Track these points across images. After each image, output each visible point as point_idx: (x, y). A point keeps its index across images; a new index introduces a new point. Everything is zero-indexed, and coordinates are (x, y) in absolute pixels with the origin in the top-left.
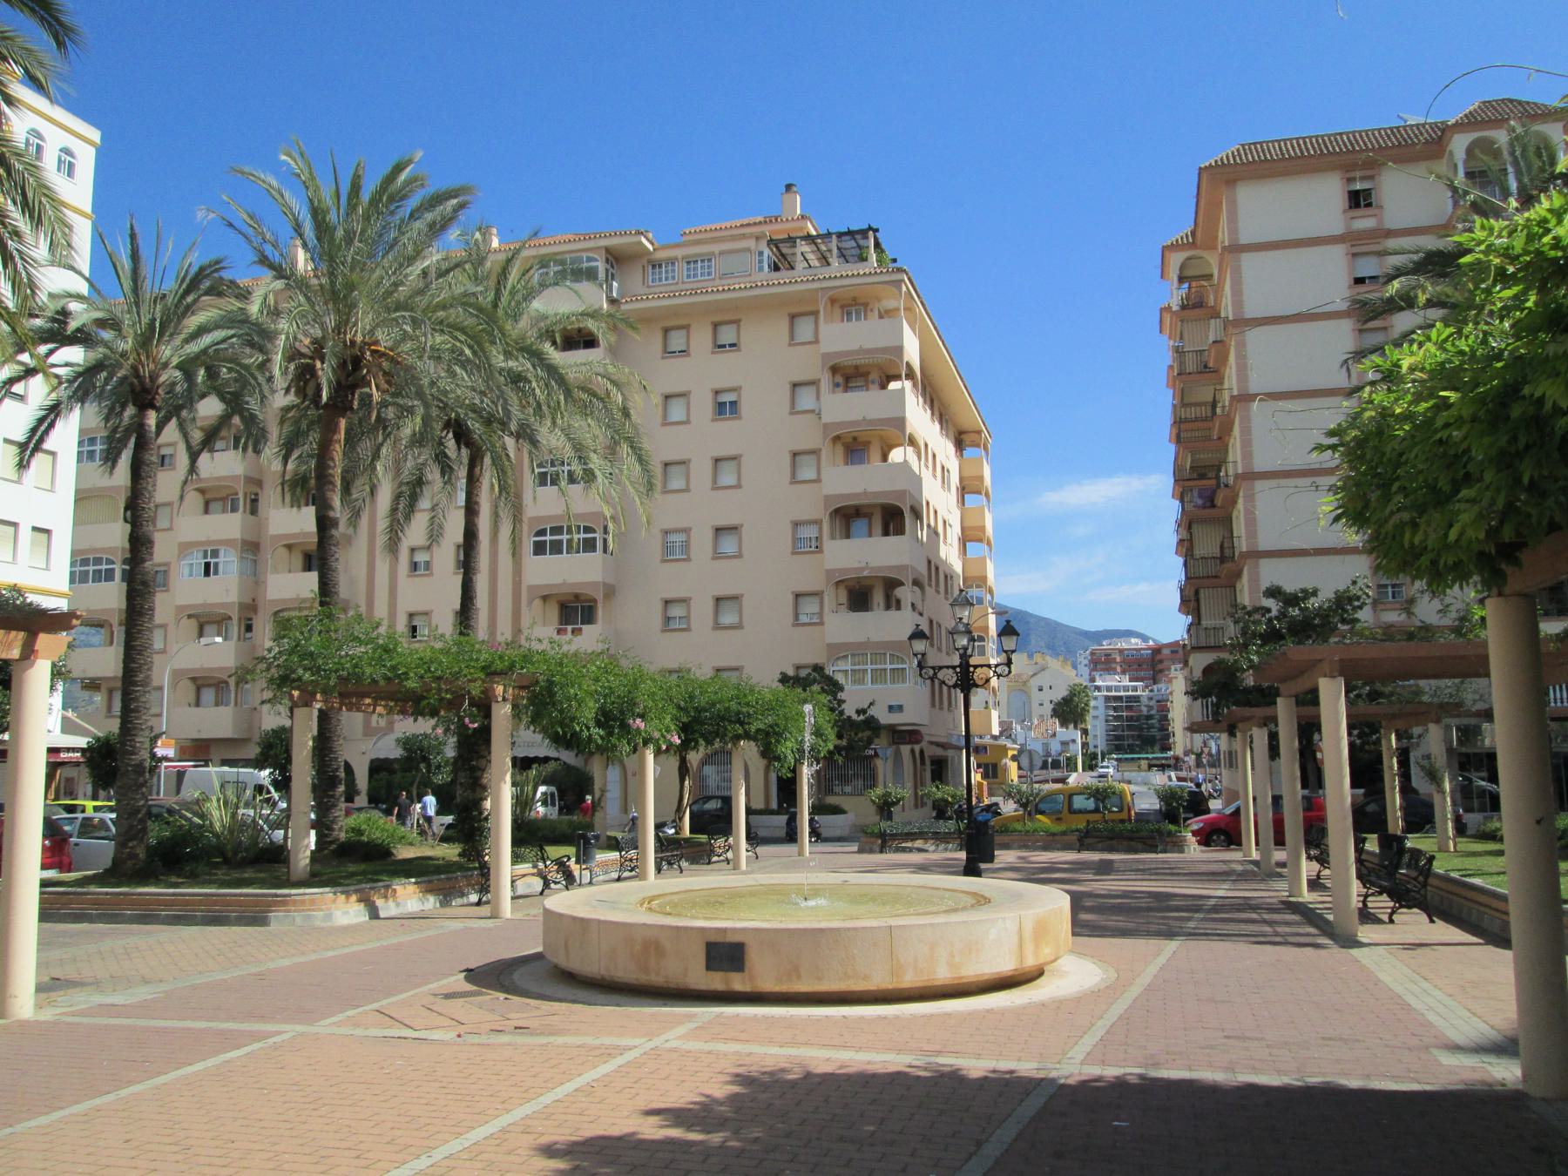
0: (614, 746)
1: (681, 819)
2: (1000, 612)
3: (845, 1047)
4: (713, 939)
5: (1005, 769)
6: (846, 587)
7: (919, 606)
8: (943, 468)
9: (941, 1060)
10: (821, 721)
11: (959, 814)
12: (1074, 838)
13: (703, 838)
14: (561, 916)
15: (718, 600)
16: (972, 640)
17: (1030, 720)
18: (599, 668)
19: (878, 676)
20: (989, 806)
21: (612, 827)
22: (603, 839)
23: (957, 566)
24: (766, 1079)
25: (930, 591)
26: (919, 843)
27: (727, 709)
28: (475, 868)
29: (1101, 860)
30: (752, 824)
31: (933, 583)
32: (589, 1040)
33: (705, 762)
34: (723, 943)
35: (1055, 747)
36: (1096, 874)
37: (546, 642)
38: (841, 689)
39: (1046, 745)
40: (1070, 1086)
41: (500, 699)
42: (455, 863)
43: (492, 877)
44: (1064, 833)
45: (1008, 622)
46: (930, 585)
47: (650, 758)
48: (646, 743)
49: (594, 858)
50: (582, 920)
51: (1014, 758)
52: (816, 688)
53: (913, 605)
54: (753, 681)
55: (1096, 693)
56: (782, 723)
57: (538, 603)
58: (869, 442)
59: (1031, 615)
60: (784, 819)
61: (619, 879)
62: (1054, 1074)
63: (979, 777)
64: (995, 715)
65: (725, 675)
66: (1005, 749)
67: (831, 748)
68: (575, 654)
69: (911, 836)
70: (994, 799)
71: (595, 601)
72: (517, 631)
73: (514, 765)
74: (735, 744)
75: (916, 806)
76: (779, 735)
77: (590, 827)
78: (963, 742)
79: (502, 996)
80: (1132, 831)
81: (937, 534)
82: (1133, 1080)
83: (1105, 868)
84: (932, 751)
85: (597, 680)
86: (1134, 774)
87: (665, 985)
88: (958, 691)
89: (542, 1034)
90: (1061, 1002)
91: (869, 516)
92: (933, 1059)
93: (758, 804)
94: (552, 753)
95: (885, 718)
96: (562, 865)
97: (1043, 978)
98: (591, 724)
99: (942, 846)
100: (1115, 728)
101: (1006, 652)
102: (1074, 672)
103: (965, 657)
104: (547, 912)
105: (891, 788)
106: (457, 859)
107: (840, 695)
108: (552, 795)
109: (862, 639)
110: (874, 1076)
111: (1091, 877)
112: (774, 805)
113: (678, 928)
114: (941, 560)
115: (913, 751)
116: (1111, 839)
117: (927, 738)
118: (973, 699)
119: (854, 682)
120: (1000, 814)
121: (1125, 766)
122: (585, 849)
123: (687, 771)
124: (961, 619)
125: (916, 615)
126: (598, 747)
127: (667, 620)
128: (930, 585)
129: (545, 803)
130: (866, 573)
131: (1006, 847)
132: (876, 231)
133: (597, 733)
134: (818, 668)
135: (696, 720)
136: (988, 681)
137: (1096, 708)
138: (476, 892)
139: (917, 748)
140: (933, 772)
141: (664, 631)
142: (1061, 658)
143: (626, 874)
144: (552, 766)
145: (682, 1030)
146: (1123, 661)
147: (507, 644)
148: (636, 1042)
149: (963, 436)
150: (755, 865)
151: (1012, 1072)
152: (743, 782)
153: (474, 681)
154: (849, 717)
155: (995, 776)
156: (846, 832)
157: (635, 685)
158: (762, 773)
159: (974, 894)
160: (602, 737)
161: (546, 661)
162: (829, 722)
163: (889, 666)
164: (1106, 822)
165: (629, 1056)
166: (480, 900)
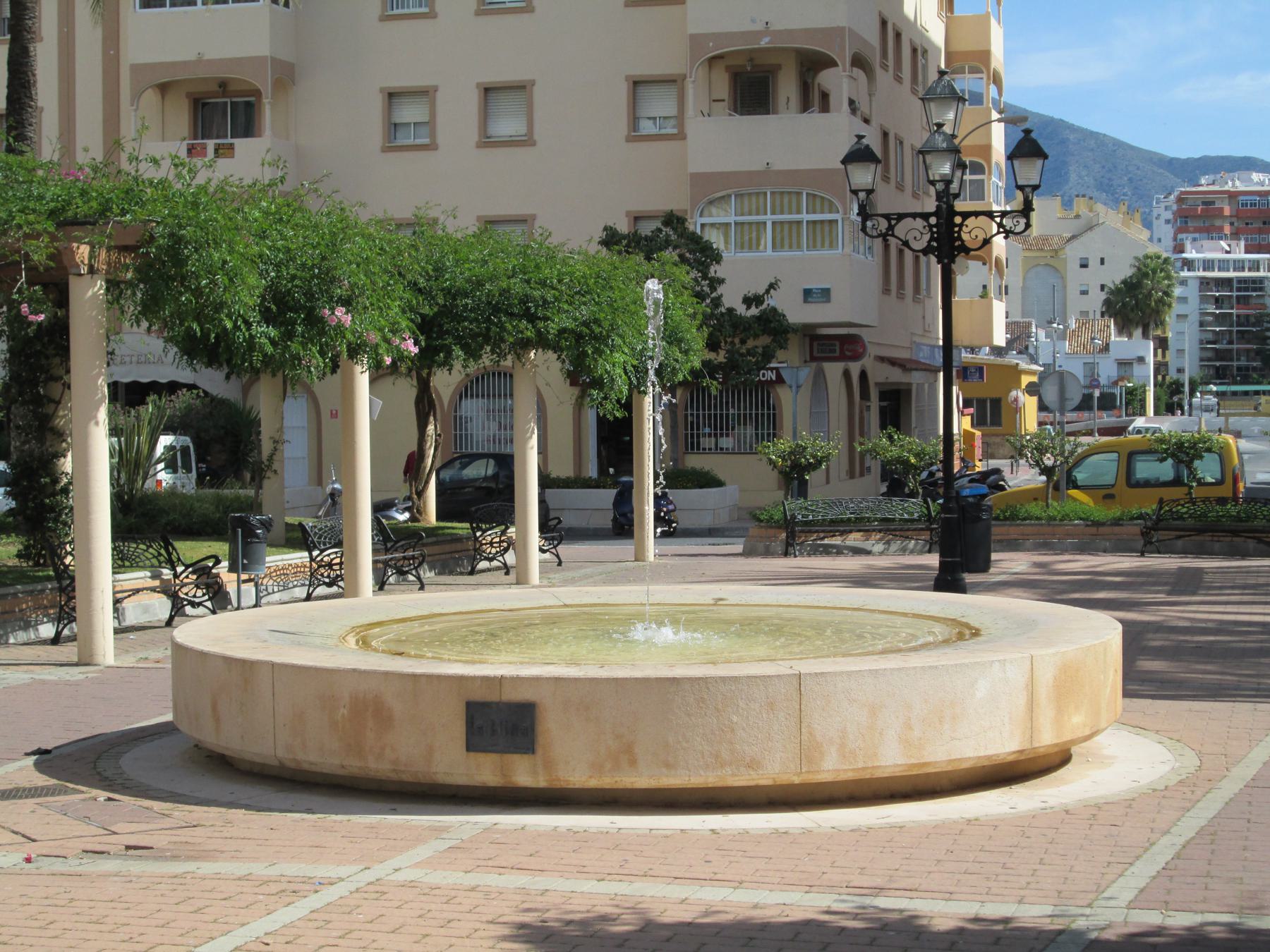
0: (297, 357)
1: (421, 493)
2: (1013, 118)
3: (714, 880)
4: (480, 695)
5: (1017, 409)
6: (728, 68)
7: (864, 108)
9: (883, 902)
10: (678, 314)
11: (930, 488)
12: (1135, 529)
13: (462, 528)
14: (203, 655)
15: (488, 91)
16: (961, 166)
17: (1064, 321)
18: (266, 213)
19: (786, 235)
20: (984, 476)
21: (294, 510)
22: (278, 530)
23: (935, 31)
24: (573, 931)
25: (884, 78)
26: (854, 539)
27: (505, 292)
28: (48, 578)
29: (1181, 569)
30: (551, 504)
31: (891, 63)
32: (259, 869)
33: (467, 390)
34: (498, 704)
35: (1107, 370)
36: (1169, 593)
37: (166, 164)
38: (717, 258)
39: (1091, 368)
40: (1108, 942)
41: (84, 269)
42: (12, 570)
43: (78, 593)
44: (1117, 522)
45: (1027, 132)
46: (884, 67)
47: (362, 380)
48: (354, 352)
49: (264, 563)
50: (243, 662)
51: (1032, 389)
52: (670, 255)
53: (851, 102)
54: (554, 241)
55: (1185, 274)
56: (605, 316)
57: (151, 97)
58: (779, 67)
59: (1072, 128)
60: (609, 495)
61: (309, 598)
62: (1080, 924)
63: (966, 423)
64: (999, 309)
65: (501, 229)
66: (1016, 372)
67: (697, 364)
68: (221, 189)
69: (840, 526)
70: (994, 463)
71: (257, 93)
72: (113, 144)
73: (113, 398)
74: (519, 357)
75: (851, 475)
76: (601, 339)
77: (254, 506)
78: (939, 360)
79: (102, 795)
80: (1238, 518)
82: (1218, 933)
83: (1187, 583)
84: (881, 375)
85: (262, 235)
86: (1246, 420)
87: (394, 776)
88: (933, 259)
89: (175, 858)
90: (1098, 807)
92: (868, 901)
93: (562, 468)
94: (184, 375)
95: (797, 313)
96: (204, 574)
97: (1069, 766)
98: (254, 317)
99: (895, 546)
100: (1216, 339)
101: (1021, 188)
102: (1145, 235)
103: (946, 196)
104: (178, 649)
105: (805, 438)
106: (14, 562)
107: (715, 270)
108: (185, 450)
109: (758, 166)
110: (765, 927)
111: (1161, 597)
112: (592, 471)
113: (415, 677)
114: (906, 19)
115: (847, 374)
116: (1200, 531)
117: (873, 351)
118: (960, 281)
119: (741, 246)
120: (1002, 488)
121: (1231, 405)
122: (246, 544)
123: (432, 405)
124: (940, 126)
125: (857, 121)
126: (268, 360)
127: (393, 128)
128: (884, 67)
129: (171, 466)
130: (764, 42)
131: (1012, 545)
133: (264, 333)
134: (674, 220)
135: (446, 312)
136: (987, 242)
137: (1183, 300)
138: (51, 620)
139: (855, 368)
140: (883, 412)
141: (386, 149)
142: (1124, 208)
143: (322, 590)
144: (183, 399)
145: (423, 852)
146: (1237, 215)
147: (95, 169)
148: (343, 871)
150: (557, 576)
151: (1006, 921)
152: (534, 427)
153: (37, 236)
154: (731, 311)
155: (996, 421)
156: (722, 520)
157: (333, 246)
158: (568, 410)
159: (954, 622)
160: (273, 342)
161: (166, 197)
162: (694, 316)
164: (1193, 501)
165: (329, 895)
166: (58, 634)
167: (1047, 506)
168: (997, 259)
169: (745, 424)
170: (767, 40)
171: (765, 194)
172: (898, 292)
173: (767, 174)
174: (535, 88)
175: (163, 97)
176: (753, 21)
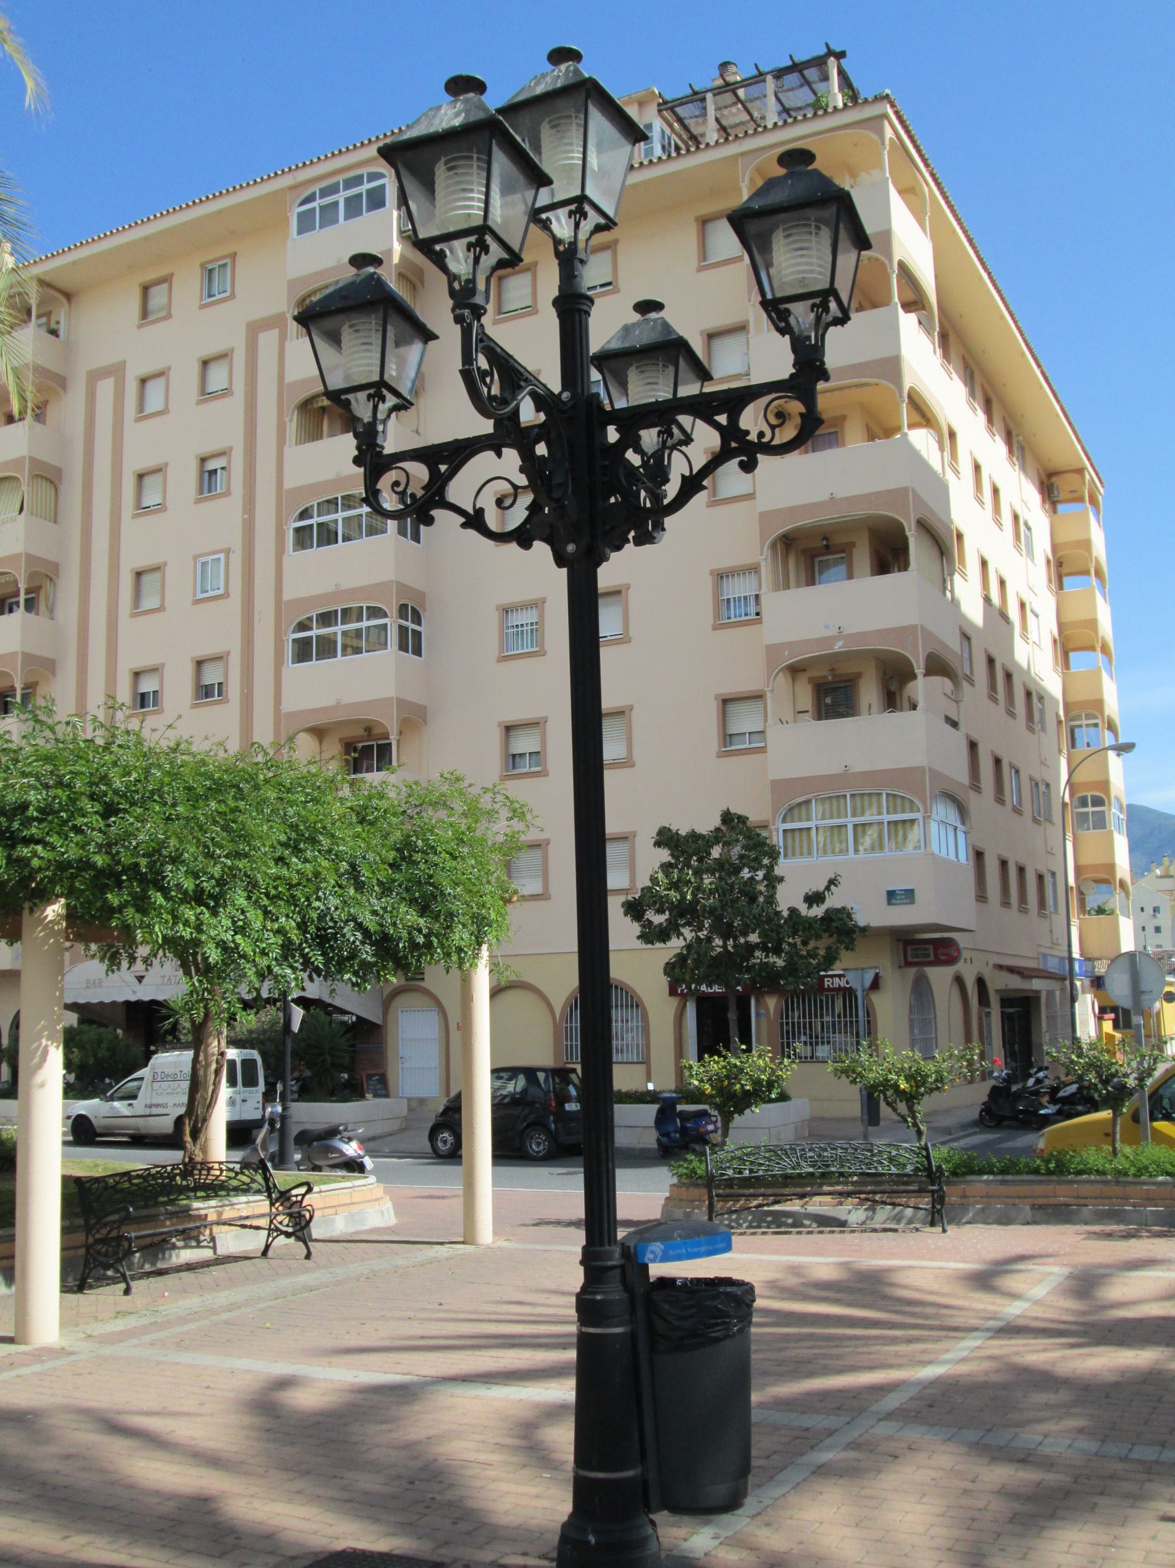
8: (1016, 518)
26: (819, 1205)
58: (859, 675)
81: (1004, 616)
91: (846, 550)
109: (835, 769)
115: (959, 980)
130: (838, 647)
132: (840, 55)
149: (1054, 479)
163: (887, 818)
167: (1114, 1153)
168: (1121, 881)
169: (846, 1032)
170: (840, 644)
171: (845, 796)
172: (1020, 906)
173: (845, 777)
174: (633, 712)
175: (321, 743)
176: (827, 627)
